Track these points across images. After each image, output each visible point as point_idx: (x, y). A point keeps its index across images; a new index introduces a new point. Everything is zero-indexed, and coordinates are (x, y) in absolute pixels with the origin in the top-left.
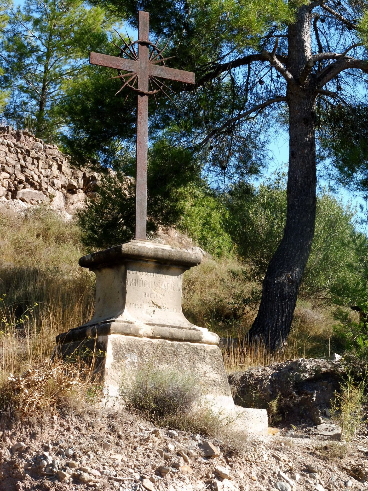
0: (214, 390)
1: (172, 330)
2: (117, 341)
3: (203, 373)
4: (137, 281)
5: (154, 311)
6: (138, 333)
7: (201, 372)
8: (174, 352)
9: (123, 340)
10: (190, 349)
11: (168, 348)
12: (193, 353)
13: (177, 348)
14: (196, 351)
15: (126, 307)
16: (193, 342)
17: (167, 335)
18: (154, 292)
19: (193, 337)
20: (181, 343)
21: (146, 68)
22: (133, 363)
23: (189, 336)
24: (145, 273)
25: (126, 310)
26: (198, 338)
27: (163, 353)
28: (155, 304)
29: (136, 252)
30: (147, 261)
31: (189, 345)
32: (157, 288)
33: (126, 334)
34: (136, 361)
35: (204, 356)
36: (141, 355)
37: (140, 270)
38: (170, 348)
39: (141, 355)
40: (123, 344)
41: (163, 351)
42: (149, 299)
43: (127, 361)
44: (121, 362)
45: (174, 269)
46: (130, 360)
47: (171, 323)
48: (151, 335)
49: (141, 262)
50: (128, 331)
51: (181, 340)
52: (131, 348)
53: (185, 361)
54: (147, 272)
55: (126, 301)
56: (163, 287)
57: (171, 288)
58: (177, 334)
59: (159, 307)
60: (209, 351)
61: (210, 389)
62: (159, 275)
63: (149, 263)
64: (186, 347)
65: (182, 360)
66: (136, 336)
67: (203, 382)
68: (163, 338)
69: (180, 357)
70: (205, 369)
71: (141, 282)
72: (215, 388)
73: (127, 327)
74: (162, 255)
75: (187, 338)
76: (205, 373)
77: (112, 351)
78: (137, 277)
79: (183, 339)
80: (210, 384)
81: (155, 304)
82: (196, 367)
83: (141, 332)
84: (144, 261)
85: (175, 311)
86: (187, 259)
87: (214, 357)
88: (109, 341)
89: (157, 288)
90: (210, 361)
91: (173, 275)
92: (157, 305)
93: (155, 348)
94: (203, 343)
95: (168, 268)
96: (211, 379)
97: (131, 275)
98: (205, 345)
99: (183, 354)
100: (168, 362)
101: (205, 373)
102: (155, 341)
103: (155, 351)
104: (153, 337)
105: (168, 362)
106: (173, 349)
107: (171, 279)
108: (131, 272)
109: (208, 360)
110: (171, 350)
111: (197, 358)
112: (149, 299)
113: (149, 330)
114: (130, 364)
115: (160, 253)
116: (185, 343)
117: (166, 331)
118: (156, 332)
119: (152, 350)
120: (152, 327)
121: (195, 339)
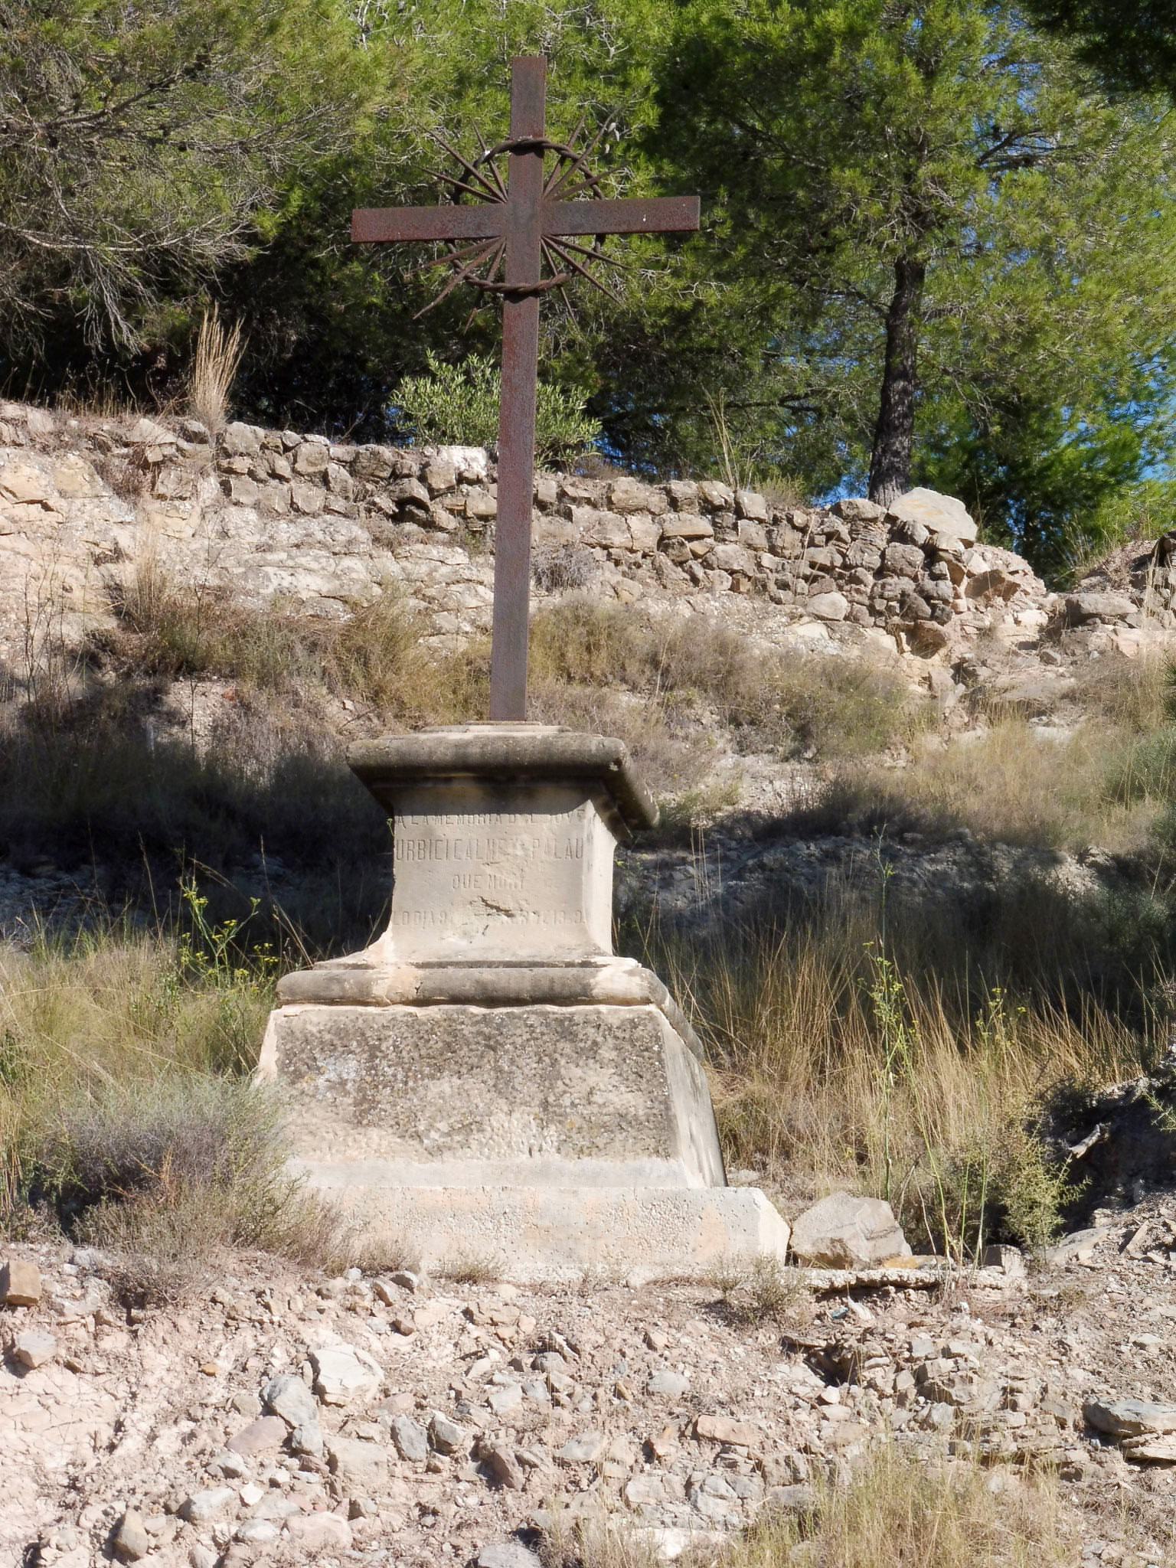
0: (617, 1144)
1: (487, 975)
2: (296, 1024)
3: (584, 1094)
4: (429, 843)
6: (368, 994)
7: (579, 1090)
8: (488, 1038)
9: (315, 1020)
10: (548, 1025)
11: (467, 1030)
12: (556, 1037)
13: (499, 1027)
14: (566, 1031)
16: (572, 1004)
17: (469, 988)
18: (488, 870)
19: (557, 988)
20: (516, 1010)
21: (532, 216)
22: (343, 1083)
23: (545, 985)
25: (386, 936)
26: (578, 988)
27: (448, 1045)
29: (394, 759)
30: (448, 780)
31: (545, 1014)
32: (498, 857)
33: (332, 1002)
34: (353, 1075)
35: (595, 1043)
36: (373, 1057)
37: (438, 810)
38: (474, 1029)
39: (373, 1057)
40: (314, 1030)
41: (449, 1039)
43: (321, 1081)
44: (303, 1085)
45: (548, 793)
46: (333, 1076)
47: (523, 954)
48: (413, 994)
49: (429, 785)
50: (335, 991)
51: (518, 1001)
52: (338, 1042)
53: (521, 1062)
55: (394, 908)
56: (520, 852)
57: (548, 853)
58: (503, 983)
60: (616, 1023)
61: (600, 1141)
62: (505, 817)
63: (456, 786)
64: (533, 1020)
65: (512, 1061)
66: (366, 1004)
67: (578, 1121)
68: (455, 1000)
69: (506, 1052)
70: (592, 1080)
71: (442, 845)
72: (620, 1137)
74: (483, 754)
75: (538, 994)
76: (591, 1093)
77: (276, 1056)
79: (525, 995)
80: (604, 1126)
82: (559, 1077)
83: (379, 990)
84: (436, 780)
85: (560, 916)
86: (568, 755)
87: (632, 1042)
88: (271, 1025)
89: (498, 857)
90: (613, 1054)
91: (552, 811)
92: (498, 909)
93: (421, 1033)
94: (600, 1002)
95: (530, 794)
96: (611, 1109)
98: (603, 1008)
99: (519, 1041)
100: (464, 1070)
101: (591, 1093)
102: (433, 1011)
103: (421, 1043)
104: (421, 1002)
105: (464, 1070)
106: (486, 1030)
108: (408, 819)
109: (607, 1053)
110: (480, 1033)
111: (568, 1051)
114: (330, 1088)
115: (475, 750)
116: (537, 1007)
117: (463, 980)
118: (429, 984)
119: (410, 1041)
120: (421, 972)
121: (566, 992)
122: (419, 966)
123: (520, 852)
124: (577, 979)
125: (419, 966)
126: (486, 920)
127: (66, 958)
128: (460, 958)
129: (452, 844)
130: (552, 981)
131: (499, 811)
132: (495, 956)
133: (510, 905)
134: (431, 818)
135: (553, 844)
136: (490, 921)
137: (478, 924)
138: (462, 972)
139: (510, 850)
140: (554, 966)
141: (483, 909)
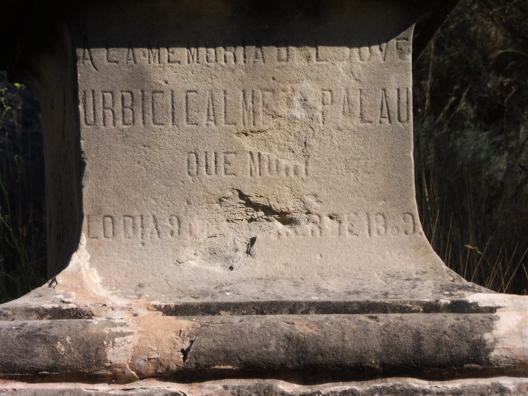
1: (303, 326)
4: (142, 97)
5: (253, 241)
6: (100, 361)
15: (84, 239)
16: (451, 377)
17: (274, 347)
18: (247, 143)
19: (428, 347)
23: (406, 342)
24: (182, 53)
25: (80, 259)
26: (465, 349)
28: (257, 207)
32: (264, 121)
42: (218, 182)
47: (335, 289)
50: (41, 356)
54: (193, 42)
56: (299, 113)
57: (349, 113)
58: (333, 341)
59: (285, 218)
62: (272, 52)
73: (32, 336)
78: (140, 76)
81: (257, 207)
83: (118, 355)
85: (378, 224)
89: (264, 121)
92: (268, 210)
97: (100, 70)
107: (340, 66)
108: (101, 54)
112: (218, 182)
113: (168, 338)
117: (266, 333)
118: (205, 343)
120: (185, 323)
121: (443, 356)
122: (168, 311)
123: (299, 113)
124: (460, 332)
125: (168, 311)
126: (247, 231)
127: (169, 366)
128: (229, 297)
129: (180, 98)
130: (418, 337)
131: (260, 42)
132: (288, 293)
133: (287, 203)
134: (142, 55)
135: (356, 98)
136: (255, 230)
137: (235, 236)
138: (257, 322)
139: (283, 110)
140: (403, 309)
141: (240, 210)
